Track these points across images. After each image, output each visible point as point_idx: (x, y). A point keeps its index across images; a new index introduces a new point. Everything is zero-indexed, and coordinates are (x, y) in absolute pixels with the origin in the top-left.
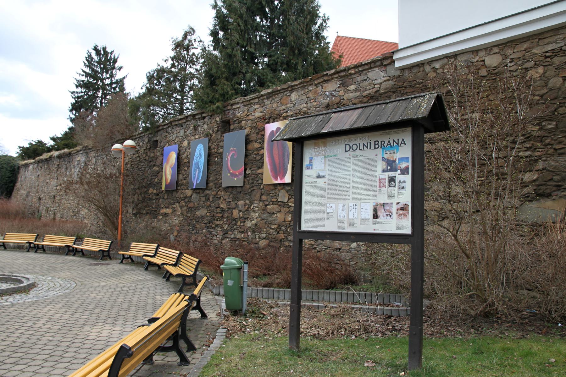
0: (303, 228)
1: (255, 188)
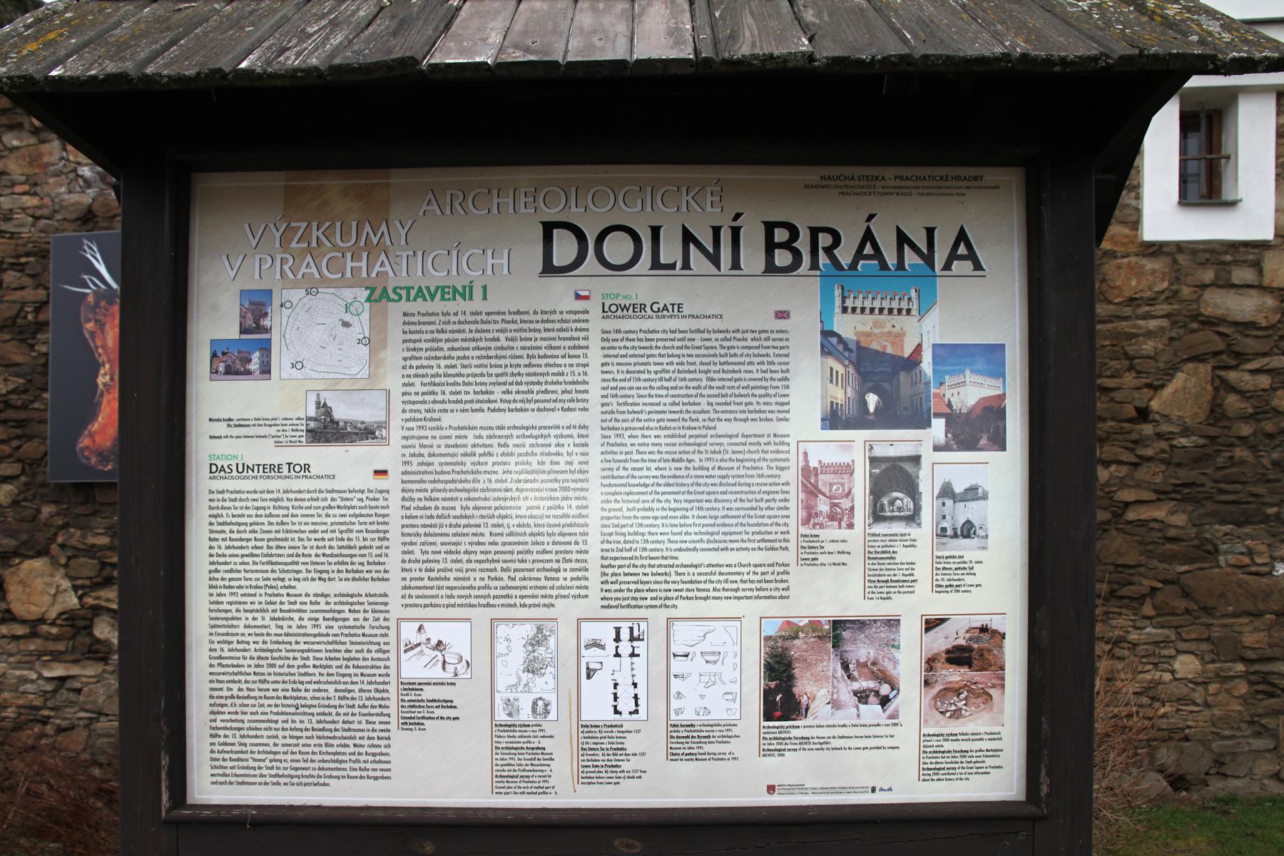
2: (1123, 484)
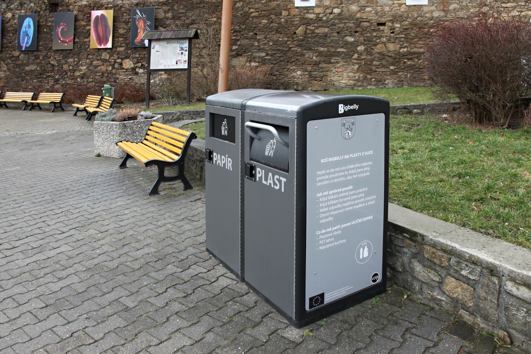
0: (151, 68)
1: (82, 51)
2: (291, 44)
